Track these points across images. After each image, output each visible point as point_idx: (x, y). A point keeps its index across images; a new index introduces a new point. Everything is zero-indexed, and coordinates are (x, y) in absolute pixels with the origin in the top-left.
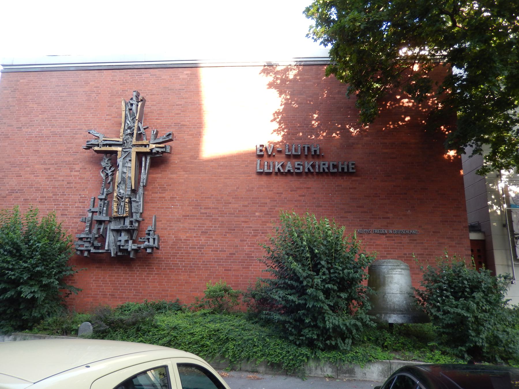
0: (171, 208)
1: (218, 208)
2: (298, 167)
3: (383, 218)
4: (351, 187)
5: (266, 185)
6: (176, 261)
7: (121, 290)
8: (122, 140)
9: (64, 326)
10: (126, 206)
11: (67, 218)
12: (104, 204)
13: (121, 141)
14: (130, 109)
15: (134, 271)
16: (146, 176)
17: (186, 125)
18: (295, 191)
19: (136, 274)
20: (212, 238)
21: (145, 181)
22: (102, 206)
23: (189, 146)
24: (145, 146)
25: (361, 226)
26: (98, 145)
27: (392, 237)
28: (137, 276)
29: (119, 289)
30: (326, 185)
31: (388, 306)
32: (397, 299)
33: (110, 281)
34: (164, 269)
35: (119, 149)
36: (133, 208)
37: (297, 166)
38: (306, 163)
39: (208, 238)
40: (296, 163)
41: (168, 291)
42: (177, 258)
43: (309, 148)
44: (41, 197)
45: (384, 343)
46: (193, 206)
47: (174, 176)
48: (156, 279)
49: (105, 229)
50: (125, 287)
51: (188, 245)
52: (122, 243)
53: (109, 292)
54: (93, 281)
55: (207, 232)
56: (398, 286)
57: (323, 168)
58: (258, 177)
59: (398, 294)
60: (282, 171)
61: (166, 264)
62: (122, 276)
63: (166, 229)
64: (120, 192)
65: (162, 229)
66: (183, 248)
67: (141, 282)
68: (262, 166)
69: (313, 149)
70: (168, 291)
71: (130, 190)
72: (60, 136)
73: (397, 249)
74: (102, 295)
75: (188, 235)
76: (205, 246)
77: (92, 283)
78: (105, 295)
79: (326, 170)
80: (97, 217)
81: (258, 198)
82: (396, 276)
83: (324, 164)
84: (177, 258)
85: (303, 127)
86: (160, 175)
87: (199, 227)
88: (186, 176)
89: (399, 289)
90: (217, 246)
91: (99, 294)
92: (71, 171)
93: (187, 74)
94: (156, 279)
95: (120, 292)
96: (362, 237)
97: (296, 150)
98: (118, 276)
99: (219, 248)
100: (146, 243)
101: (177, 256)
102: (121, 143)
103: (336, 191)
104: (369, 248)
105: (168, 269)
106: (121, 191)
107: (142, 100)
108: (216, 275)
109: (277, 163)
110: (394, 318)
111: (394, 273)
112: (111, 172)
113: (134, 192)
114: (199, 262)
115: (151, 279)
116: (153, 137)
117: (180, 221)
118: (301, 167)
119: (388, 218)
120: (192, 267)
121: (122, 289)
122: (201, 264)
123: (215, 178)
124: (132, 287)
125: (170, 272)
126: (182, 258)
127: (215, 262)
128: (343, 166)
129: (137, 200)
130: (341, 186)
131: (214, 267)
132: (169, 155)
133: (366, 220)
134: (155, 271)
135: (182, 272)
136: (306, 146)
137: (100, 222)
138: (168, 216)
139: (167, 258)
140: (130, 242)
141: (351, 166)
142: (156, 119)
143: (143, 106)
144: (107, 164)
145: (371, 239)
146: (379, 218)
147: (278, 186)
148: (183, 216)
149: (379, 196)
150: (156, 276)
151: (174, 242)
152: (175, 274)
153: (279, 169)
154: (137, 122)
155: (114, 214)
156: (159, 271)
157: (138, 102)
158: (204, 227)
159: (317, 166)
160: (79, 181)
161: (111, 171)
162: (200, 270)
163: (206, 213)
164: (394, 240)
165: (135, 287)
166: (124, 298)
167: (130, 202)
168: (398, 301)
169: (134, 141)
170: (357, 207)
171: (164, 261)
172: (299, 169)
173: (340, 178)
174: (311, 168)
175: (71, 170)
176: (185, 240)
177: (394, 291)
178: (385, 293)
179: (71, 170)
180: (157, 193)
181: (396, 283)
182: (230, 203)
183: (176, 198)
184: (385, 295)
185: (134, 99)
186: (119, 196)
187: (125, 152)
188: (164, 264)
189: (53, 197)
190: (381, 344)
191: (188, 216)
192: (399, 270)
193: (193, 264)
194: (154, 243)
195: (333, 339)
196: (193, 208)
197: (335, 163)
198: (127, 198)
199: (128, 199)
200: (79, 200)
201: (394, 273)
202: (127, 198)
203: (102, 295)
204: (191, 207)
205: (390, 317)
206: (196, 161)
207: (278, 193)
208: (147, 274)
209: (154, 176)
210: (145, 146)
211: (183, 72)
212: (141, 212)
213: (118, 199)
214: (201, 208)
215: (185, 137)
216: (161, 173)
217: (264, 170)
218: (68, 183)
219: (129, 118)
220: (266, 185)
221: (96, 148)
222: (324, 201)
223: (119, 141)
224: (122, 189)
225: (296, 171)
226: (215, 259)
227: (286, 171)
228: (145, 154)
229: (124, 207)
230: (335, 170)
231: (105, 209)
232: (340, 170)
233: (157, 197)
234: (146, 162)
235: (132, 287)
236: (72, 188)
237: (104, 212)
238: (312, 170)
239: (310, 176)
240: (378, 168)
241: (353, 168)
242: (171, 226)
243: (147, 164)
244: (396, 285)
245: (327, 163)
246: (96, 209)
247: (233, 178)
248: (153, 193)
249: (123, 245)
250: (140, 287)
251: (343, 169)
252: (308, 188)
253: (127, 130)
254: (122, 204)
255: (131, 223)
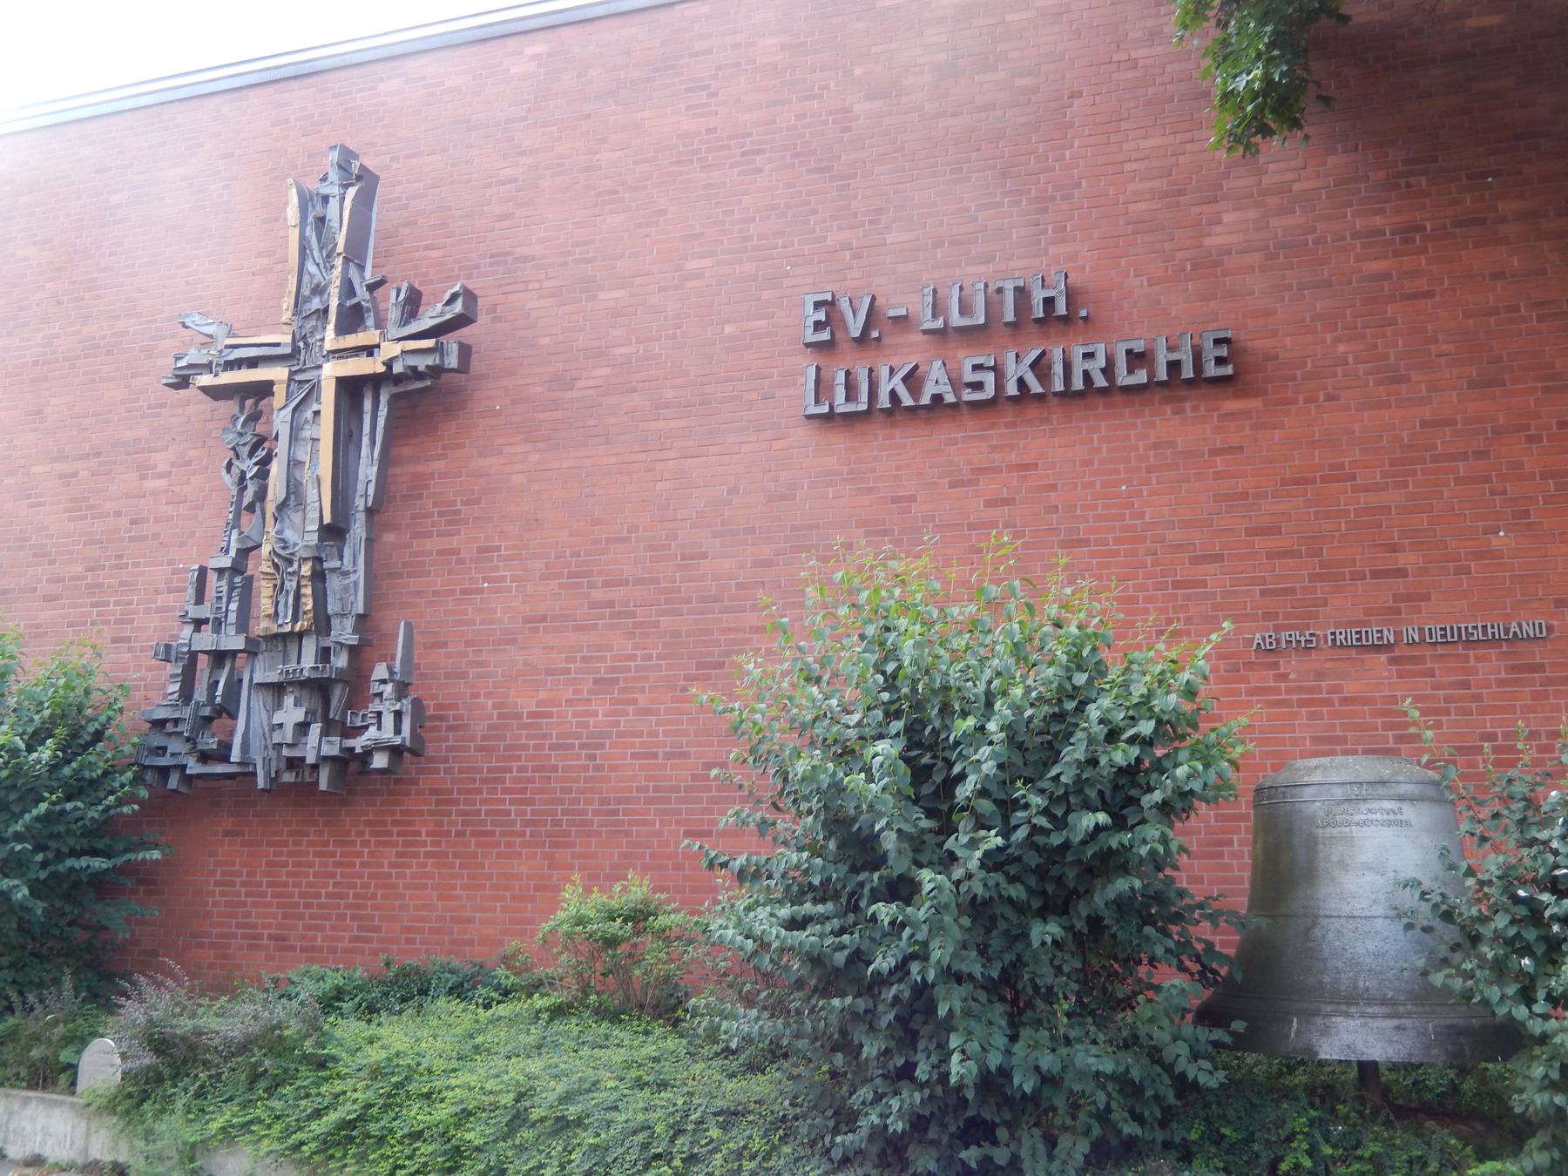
0: (481, 591)
1: (655, 581)
2: (977, 377)
3: (1376, 574)
4: (1218, 445)
5: (846, 469)
6: (501, 802)
7: (307, 921)
8: (288, 339)
9: (35, 1053)
10: (303, 591)
11: (130, 650)
12: (232, 588)
13: (286, 344)
14: (321, 220)
15: (353, 843)
16: (375, 469)
17: (533, 258)
18: (969, 483)
19: (360, 855)
20: (634, 702)
21: (371, 491)
22: (224, 594)
23: (544, 341)
24: (370, 350)
25: (1268, 616)
26: (208, 367)
27: (1420, 660)
28: (363, 865)
29: (301, 917)
30: (1104, 447)
31: (1327, 979)
32: (1371, 946)
33: (270, 884)
34: (459, 834)
35: (278, 373)
36: (330, 599)
37: (970, 376)
38: (1011, 356)
39: (619, 702)
40: (968, 365)
41: (470, 920)
42: (506, 791)
43: (1022, 293)
44: (49, 581)
45: (1279, 1159)
46: (560, 575)
47: (491, 463)
48: (430, 876)
49: (234, 686)
50: (320, 906)
51: (544, 736)
52: (288, 735)
53: (269, 926)
54: (217, 884)
55: (615, 681)
56: (1382, 880)
57: (1086, 374)
58: (838, 446)
59: (1380, 923)
60: (907, 401)
61: (466, 813)
62: (312, 865)
63: (464, 675)
64: (283, 540)
65: (448, 675)
66: (526, 747)
67: (377, 887)
68: (822, 388)
69: (1038, 296)
70: (470, 920)
71: (316, 527)
72: (109, 353)
73: (1447, 712)
74: (244, 936)
75: (543, 695)
76: (608, 735)
77: (212, 894)
78: (253, 937)
79: (1100, 381)
80: (206, 640)
81: (817, 526)
82: (1367, 831)
83: (1089, 356)
84: (506, 791)
85: (1001, 204)
86: (439, 465)
87: (585, 659)
88: (535, 457)
89: (1382, 897)
90: (656, 734)
91: (234, 936)
92: (143, 477)
93: (535, 57)
94: (430, 876)
95: (307, 927)
96: (1276, 665)
97: (965, 309)
98: (299, 864)
99: (664, 744)
100: (372, 732)
101: (503, 780)
102: (288, 350)
103: (1149, 470)
104: (1313, 716)
105: (473, 834)
106: (289, 535)
107: (359, 178)
108: (653, 856)
109: (884, 372)
110: (1346, 1038)
111: (1357, 818)
112: (255, 464)
113: (334, 532)
114: (587, 802)
115: (413, 877)
116: (393, 315)
117: (513, 642)
118: (989, 379)
119: (1402, 573)
120: (557, 823)
121: (312, 916)
122: (596, 813)
123: (642, 456)
124: (348, 907)
125: (478, 845)
126: (524, 791)
127: (650, 801)
128: (1174, 356)
129: (348, 565)
130: (1173, 444)
131: (645, 823)
132: (460, 379)
133: (1292, 591)
134: (424, 844)
135: (522, 845)
136: (1009, 286)
137: (219, 657)
138: (473, 622)
139: (469, 791)
140: (316, 729)
141: (1210, 352)
142: (426, 248)
143: (365, 201)
144: (241, 434)
145: (1320, 675)
146: (1357, 576)
147: (898, 468)
148: (526, 621)
149: (1353, 477)
150: (430, 861)
151: (491, 727)
152: (499, 855)
153: (893, 394)
154: (339, 262)
155: (262, 626)
156: (438, 844)
157: (346, 187)
158: (602, 659)
159: (1058, 369)
160: (170, 510)
161: (254, 460)
162: (589, 834)
163: (611, 604)
164: (1430, 673)
165: (358, 907)
166: (320, 950)
167: (319, 576)
168: (1376, 955)
169: (330, 340)
170: (1251, 532)
171: (455, 802)
172: (978, 386)
173: (1168, 409)
174: (1031, 379)
175: (143, 471)
176: (531, 715)
177: (1359, 907)
178: (1316, 916)
179: (143, 471)
180: (429, 535)
181: (1367, 867)
182: (705, 556)
183: (498, 548)
184: (1314, 924)
185: (334, 176)
186: (279, 556)
187: (300, 382)
188: (460, 813)
189: (86, 578)
190: (1264, 1161)
191: (544, 619)
192: (1388, 805)
193: (565, 812)
194: (398, 731)
195: (1002, 1134)
196: (561, 586)
197: (1138, 346)
198: (305, 559)
199: (310, 564)
200: (168, 581)
201: (1357, 818)
202: (305, 559)
203: (244, 936)
204: (554, 583)
205: (1326, 1031)
206: (570, 395)
207: (895, 500)
208: (399, 855)
209: (420, 468)
210: (370, 350)
211: (521, 52)
212: (361, 611)
213: (276, 566)
214: (591, 586)
215: (530, 305)
216: (443, 457)
217: (831, 407)
218: (133, 522)
219: (316, 254)
220: (846, 469)
221: (205, 380)
222: (1097, 518)
223: (278, 345)
224: (293, 527)
225: (968, 395)
226: (644, 789)
227: (926, 400)
228: (375, 381)
229: (298, 596)
230: (1141, 377)
231: (233, 606)
232: (1162, 375)
233: (429, 553)
234: (376, 415)
235: (348, 907)
236: (145, 538)
237: (232, 618)
238: (1036, 387)
239: (1033, 412)
240: (1342, 348)
241: (1220, 361)
242: (481, 664)
243: (381, 422)
244: (1369, 877)
245: (1101, 350)
246: (205, 611)
247: (713, 450)
248: (416, 536)
249: (289, 741)
250: (375, 907)
251: (1174, 366)
252: (1026, 467)
253: (308, 300)
254: (291, 585)
255: (324, 654)
